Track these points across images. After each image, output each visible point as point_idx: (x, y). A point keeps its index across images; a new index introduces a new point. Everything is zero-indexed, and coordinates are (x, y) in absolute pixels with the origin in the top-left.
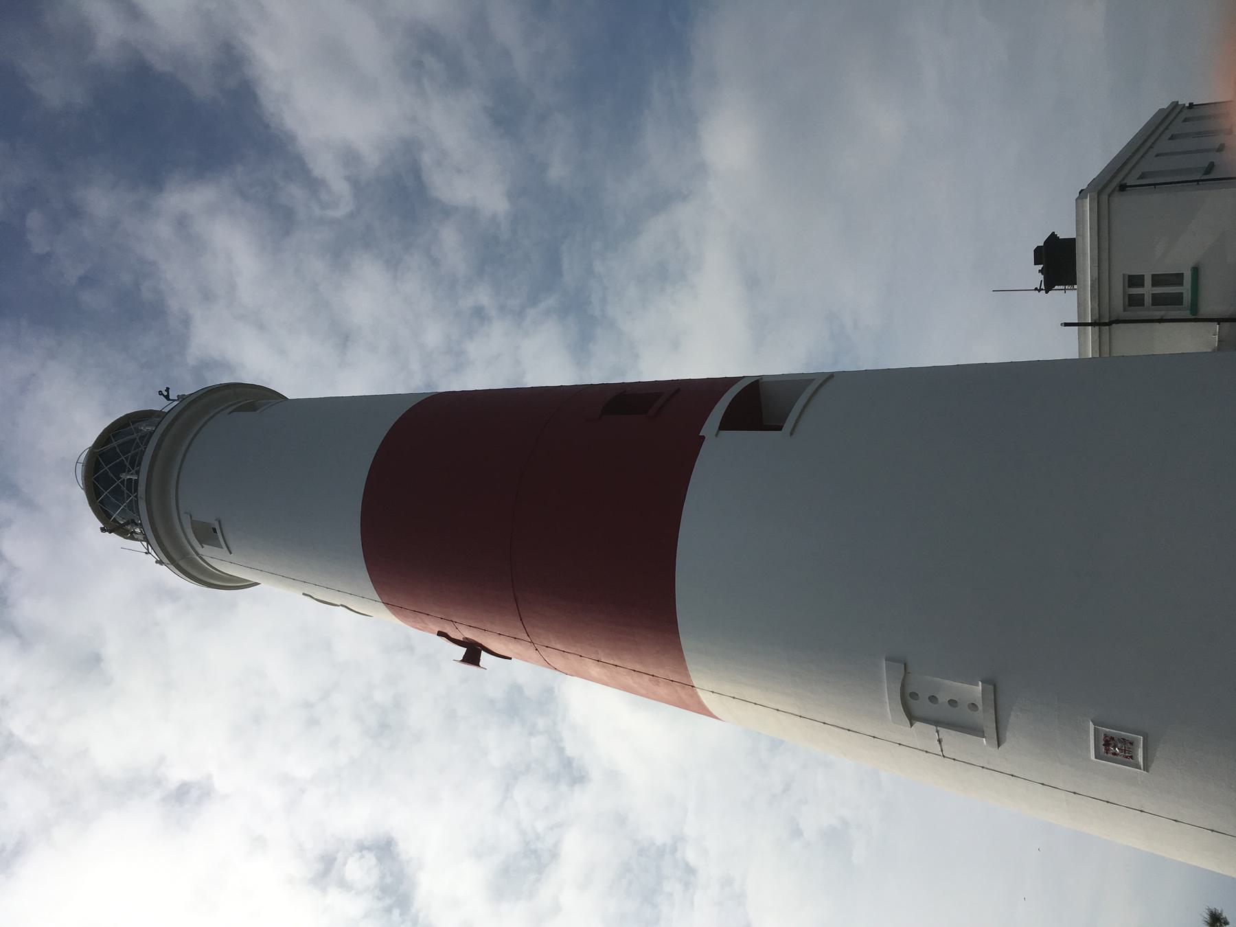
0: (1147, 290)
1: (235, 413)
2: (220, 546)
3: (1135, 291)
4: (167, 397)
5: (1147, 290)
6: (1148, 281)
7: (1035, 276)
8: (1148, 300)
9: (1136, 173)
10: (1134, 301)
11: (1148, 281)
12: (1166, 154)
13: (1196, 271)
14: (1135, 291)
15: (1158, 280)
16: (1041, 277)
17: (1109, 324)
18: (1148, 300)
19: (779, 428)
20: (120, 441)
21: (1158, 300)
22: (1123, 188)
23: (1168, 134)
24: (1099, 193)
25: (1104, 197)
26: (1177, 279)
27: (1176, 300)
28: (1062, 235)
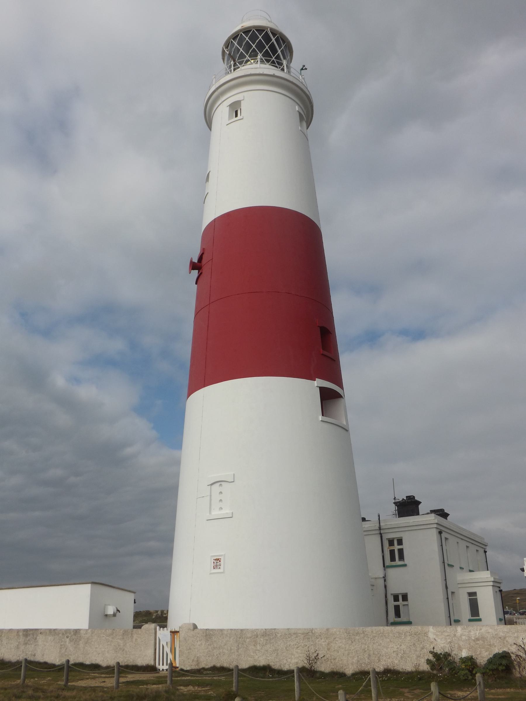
0: (396, 547)
1: (292, 65)
2: (229, 119)
3: (396, 542)
4: (302, 69)
5: (396, 547)
6: (400, 547)
7: (401, 496)
8: (392, 548)
9: (447, 536)
10: (391, 542)
11: (400, 547)
12: (387, 616)
13: (405, 565)
14: (396, 542)
15: (401, 551)
16: (401, 500)
17: (381, 534)
18: (392, 548)
19: (323, 415)
20: (275, 43)
21: (392, 552)
22: (440, 533)
23: (468, 544)
24: (437, 524)
25: (435, 526)
26: (401, 558)
27: (393, 559)
28: (420, 506)
